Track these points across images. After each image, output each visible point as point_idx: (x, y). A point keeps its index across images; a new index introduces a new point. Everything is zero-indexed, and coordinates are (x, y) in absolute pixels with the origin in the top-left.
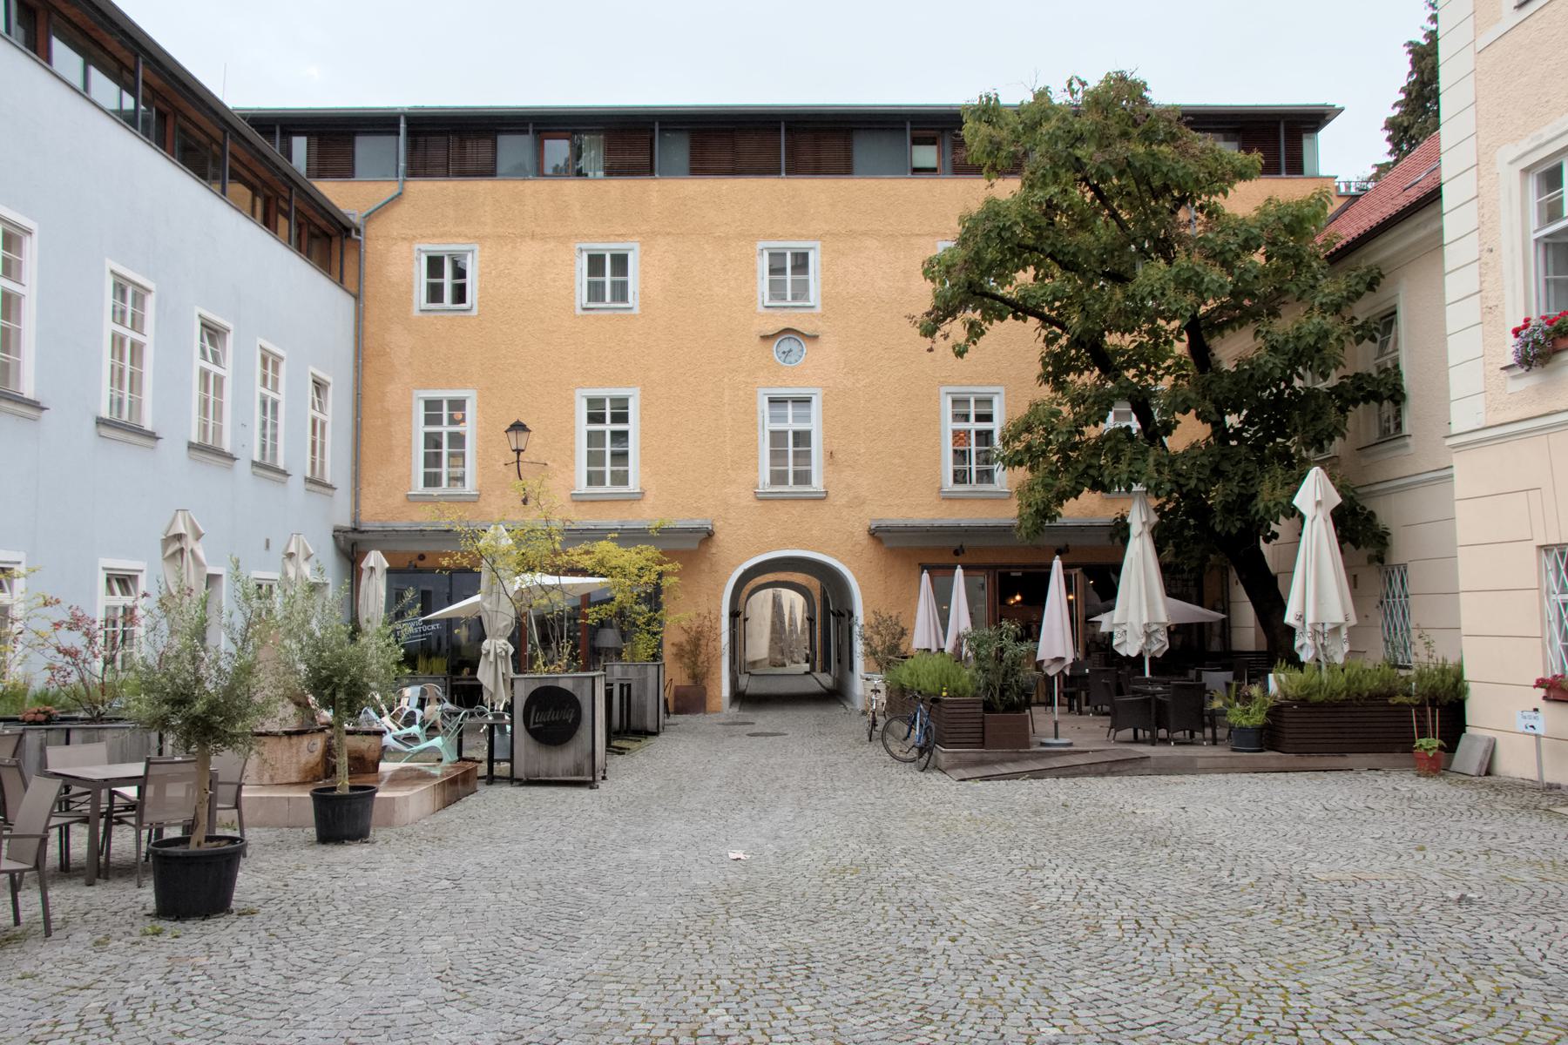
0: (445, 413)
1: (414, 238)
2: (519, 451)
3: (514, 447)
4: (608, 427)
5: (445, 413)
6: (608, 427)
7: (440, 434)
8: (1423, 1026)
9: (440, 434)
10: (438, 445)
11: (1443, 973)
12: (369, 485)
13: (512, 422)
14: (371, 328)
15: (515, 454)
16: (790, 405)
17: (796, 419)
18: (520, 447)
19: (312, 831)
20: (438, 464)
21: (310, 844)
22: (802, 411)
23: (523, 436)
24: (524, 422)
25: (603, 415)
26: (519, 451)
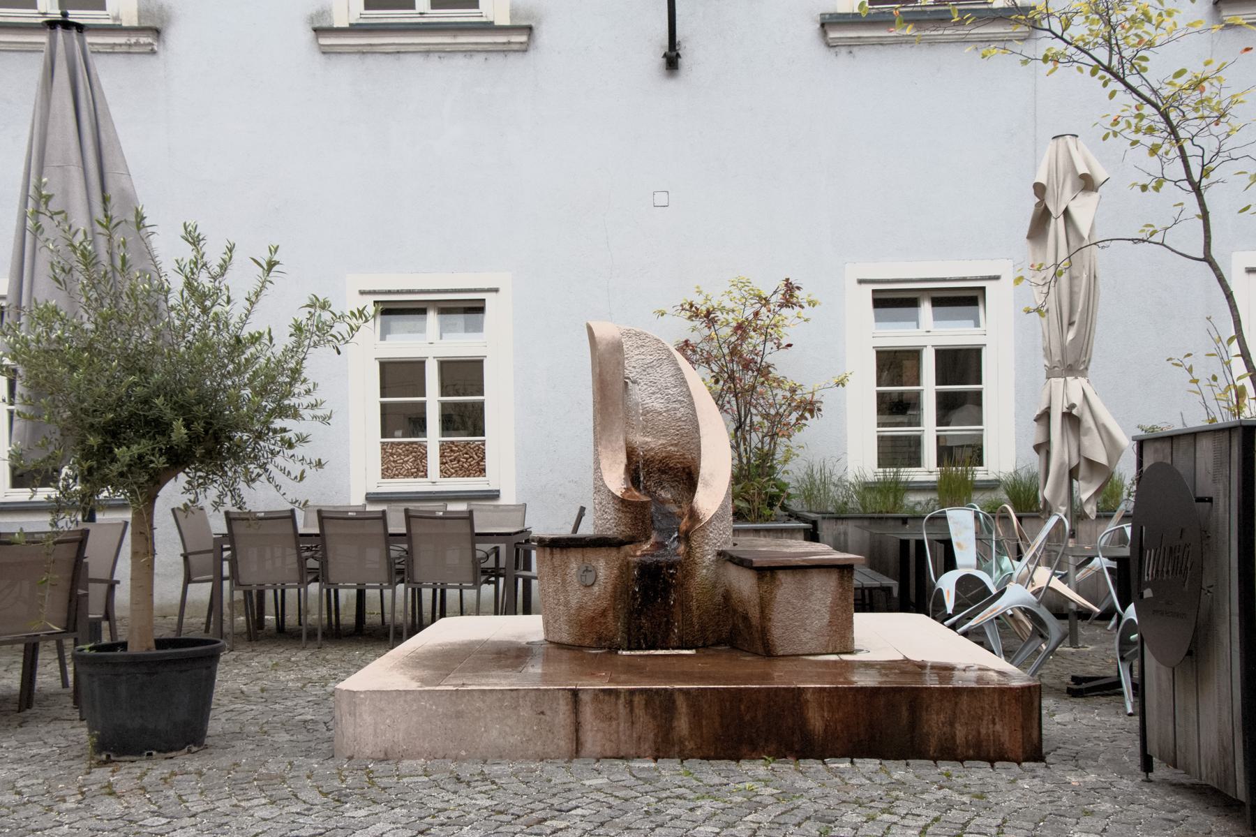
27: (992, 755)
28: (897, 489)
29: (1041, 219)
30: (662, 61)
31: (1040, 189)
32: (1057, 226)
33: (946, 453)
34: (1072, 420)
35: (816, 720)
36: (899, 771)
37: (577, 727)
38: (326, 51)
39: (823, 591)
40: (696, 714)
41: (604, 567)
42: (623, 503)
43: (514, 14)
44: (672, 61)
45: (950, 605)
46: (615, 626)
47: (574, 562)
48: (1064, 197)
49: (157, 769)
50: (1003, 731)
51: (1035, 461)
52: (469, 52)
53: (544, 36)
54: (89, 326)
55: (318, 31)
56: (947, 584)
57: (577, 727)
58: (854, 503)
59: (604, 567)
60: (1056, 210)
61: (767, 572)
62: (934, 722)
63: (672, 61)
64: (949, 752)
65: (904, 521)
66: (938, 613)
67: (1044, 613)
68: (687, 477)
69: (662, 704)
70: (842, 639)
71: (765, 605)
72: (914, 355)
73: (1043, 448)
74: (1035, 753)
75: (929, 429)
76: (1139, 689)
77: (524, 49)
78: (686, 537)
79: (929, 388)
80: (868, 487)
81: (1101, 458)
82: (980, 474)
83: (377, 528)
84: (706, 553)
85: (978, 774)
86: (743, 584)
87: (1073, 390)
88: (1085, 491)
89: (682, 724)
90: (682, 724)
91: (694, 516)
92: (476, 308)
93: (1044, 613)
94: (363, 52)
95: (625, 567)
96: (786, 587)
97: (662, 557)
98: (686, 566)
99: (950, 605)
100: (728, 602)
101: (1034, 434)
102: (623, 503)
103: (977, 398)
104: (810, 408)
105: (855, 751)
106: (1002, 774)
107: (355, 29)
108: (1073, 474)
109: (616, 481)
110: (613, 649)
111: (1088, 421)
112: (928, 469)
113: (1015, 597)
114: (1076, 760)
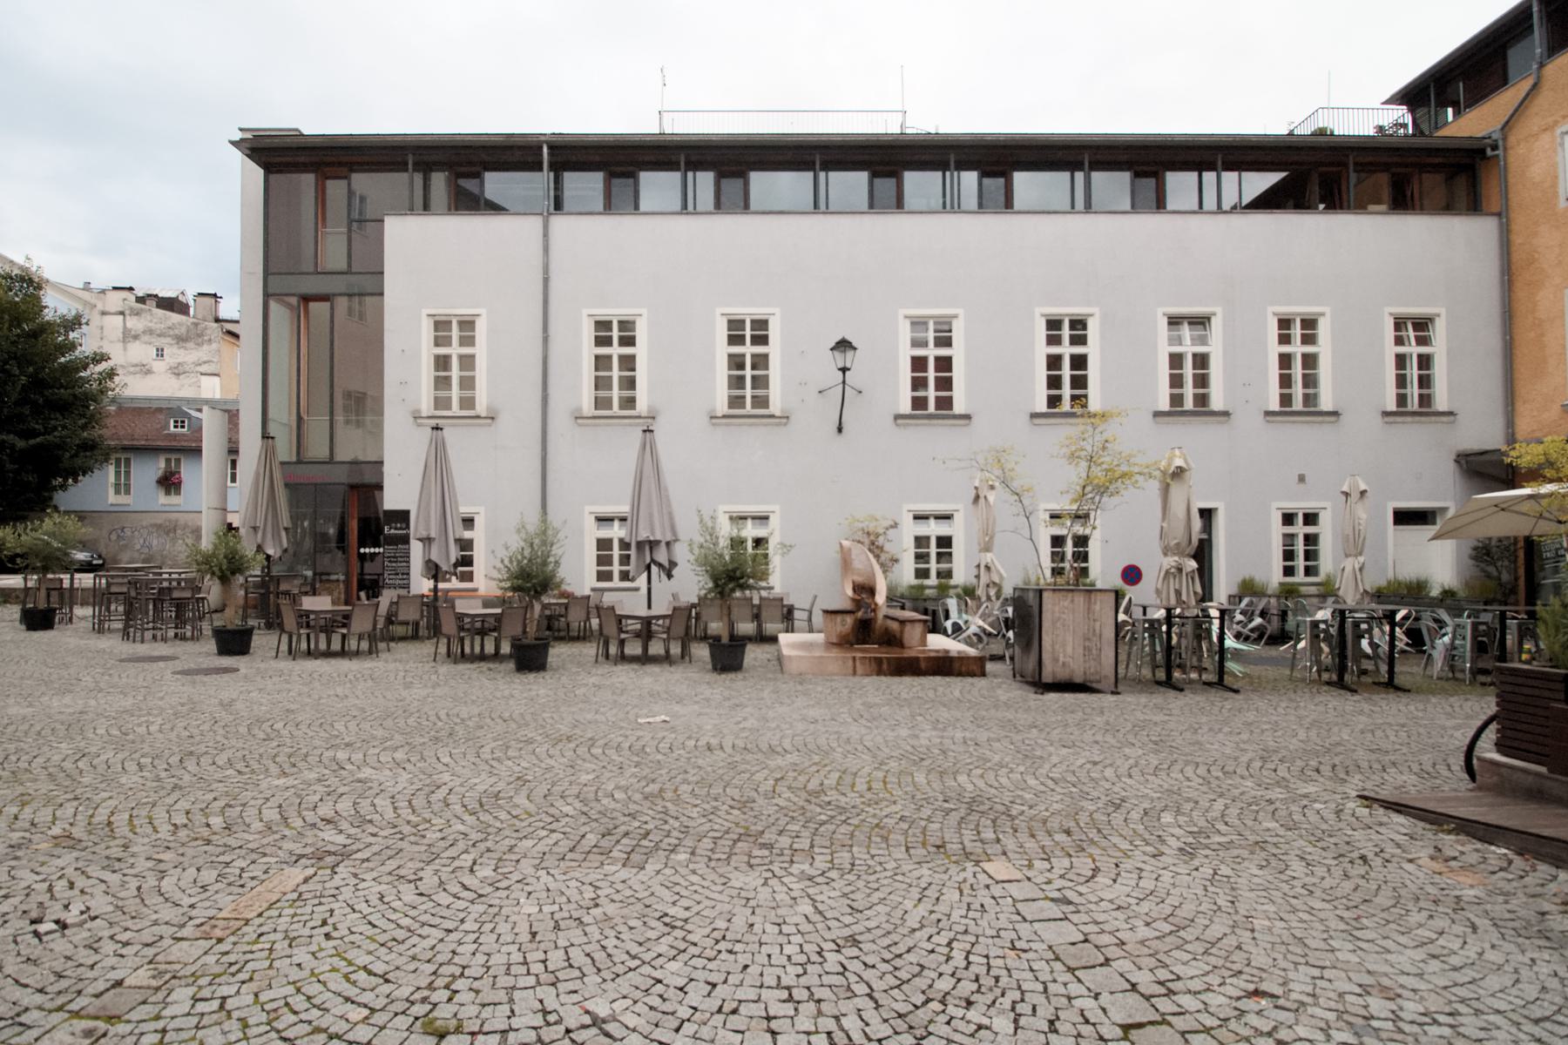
0: (748, 333)
1: (1556, 123)
2: (844, 370)
3: (841, 365)
4: (616, 351)
5: (748, 333)
6: (616, 351)
7: (743, 356)
8: (278, 901)
9: (743, 356)
10: (741, 366)
11: (736, 868)
12: (1524, 403)
13: (838, 338)
14: (1517, 239)
15: (841, 373)
16: (1186, 326)
17: (1194, 341)
18: (848, 365)
19: (710, 666)
20: (1420, 378)
21: (708, 671)
22: (1199, 332)
23: (850, 354)
24: (849, 338)
25: (743, 337)
26: (844, 370)
27: (972, 674)
28: (922, 587)
29: (977, 498)
30: (836, 430)
31: (976, 488)
32: (982, 500)
33: (939, 574)
34: (988, 568)
35: (923, 665)
36: (948, 679)
37: (855, 667)
38: (714, 425)
39: (919, 628)
40: (889, 664)
41: (849, 620)
42: (853, 600)
43: (782, 411)
44: (840, 430)
45: (950, 632)
46: (852, 638)
47: (839, 618)
48: (984, 492)
49: (732, 675)
50: (974, 668)
51: (974, 581)
52: (766, 425)
53: (792, 418)
54: (727, 558)
55: (712, 418)
56: (948, 625)
57: (855, 667)
58: (907, 593)
59: (849, 620)
60: (982, 495)
61: (903, 622)
62: (956, 665)
63: (840, 430)
64: (960, 674)
65: (925, 600)
66: (945, 633)
67: (982, 635)
68: (871, 591)
69: (879, 661)
70: (924, 642)
71: (902, 632)
72: (928, 538)
73: (978, 577)
74: (983, 674)
75: (748, 392)
76: (1012, 659)
77: (785, 424)
78: (874, 610)
79: (933, 550)
80: (912, 587)
81: (997, 581)
82: (952, 582)
83: (778, 603)
84: (880, 615)
85: (970, 680)
86: (895, 626)
87: (988, 557)
88: (992, 592)
89: (885, 666)
90: (885, 666)
91: (876, 604)
92: (767, 518)
93: (982, 635)
94: (727, 425)
95: (856, 620)
96: (908, 627)
97: (866, 617)
98: (873, 620)
99: (950, 632)
100: (887, 631)
101: (975, 572)
102: (853, 600)
103: (950, 554)
104: (896, 561)
105: (935, 673)
106: (975, 680)
107: (724, 417)
108: (988, 586)
109: (850, 592)
110: (852, 645)
111: (993, 568)
112: (933, 580)
113: (973, 629)
114: (995, 676)
